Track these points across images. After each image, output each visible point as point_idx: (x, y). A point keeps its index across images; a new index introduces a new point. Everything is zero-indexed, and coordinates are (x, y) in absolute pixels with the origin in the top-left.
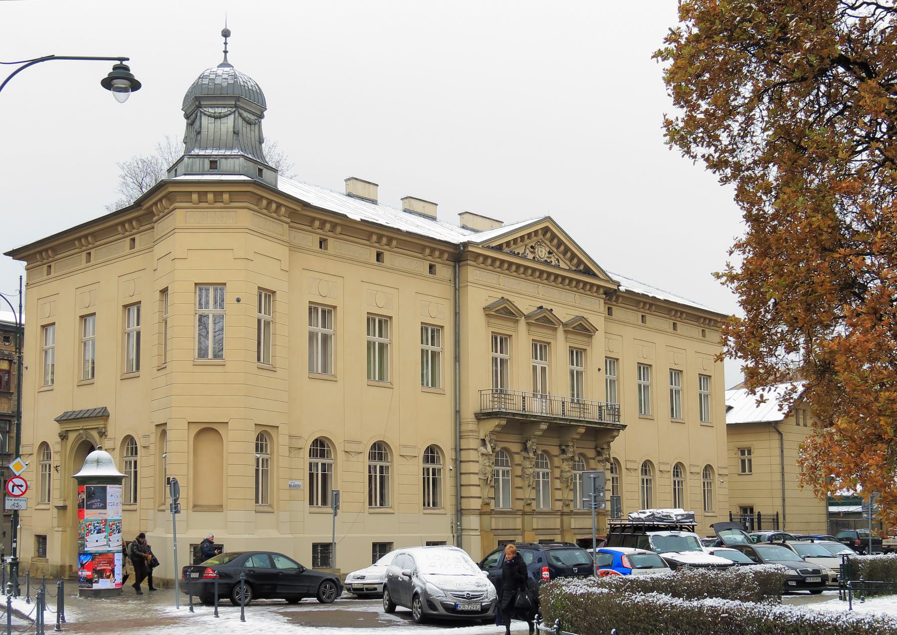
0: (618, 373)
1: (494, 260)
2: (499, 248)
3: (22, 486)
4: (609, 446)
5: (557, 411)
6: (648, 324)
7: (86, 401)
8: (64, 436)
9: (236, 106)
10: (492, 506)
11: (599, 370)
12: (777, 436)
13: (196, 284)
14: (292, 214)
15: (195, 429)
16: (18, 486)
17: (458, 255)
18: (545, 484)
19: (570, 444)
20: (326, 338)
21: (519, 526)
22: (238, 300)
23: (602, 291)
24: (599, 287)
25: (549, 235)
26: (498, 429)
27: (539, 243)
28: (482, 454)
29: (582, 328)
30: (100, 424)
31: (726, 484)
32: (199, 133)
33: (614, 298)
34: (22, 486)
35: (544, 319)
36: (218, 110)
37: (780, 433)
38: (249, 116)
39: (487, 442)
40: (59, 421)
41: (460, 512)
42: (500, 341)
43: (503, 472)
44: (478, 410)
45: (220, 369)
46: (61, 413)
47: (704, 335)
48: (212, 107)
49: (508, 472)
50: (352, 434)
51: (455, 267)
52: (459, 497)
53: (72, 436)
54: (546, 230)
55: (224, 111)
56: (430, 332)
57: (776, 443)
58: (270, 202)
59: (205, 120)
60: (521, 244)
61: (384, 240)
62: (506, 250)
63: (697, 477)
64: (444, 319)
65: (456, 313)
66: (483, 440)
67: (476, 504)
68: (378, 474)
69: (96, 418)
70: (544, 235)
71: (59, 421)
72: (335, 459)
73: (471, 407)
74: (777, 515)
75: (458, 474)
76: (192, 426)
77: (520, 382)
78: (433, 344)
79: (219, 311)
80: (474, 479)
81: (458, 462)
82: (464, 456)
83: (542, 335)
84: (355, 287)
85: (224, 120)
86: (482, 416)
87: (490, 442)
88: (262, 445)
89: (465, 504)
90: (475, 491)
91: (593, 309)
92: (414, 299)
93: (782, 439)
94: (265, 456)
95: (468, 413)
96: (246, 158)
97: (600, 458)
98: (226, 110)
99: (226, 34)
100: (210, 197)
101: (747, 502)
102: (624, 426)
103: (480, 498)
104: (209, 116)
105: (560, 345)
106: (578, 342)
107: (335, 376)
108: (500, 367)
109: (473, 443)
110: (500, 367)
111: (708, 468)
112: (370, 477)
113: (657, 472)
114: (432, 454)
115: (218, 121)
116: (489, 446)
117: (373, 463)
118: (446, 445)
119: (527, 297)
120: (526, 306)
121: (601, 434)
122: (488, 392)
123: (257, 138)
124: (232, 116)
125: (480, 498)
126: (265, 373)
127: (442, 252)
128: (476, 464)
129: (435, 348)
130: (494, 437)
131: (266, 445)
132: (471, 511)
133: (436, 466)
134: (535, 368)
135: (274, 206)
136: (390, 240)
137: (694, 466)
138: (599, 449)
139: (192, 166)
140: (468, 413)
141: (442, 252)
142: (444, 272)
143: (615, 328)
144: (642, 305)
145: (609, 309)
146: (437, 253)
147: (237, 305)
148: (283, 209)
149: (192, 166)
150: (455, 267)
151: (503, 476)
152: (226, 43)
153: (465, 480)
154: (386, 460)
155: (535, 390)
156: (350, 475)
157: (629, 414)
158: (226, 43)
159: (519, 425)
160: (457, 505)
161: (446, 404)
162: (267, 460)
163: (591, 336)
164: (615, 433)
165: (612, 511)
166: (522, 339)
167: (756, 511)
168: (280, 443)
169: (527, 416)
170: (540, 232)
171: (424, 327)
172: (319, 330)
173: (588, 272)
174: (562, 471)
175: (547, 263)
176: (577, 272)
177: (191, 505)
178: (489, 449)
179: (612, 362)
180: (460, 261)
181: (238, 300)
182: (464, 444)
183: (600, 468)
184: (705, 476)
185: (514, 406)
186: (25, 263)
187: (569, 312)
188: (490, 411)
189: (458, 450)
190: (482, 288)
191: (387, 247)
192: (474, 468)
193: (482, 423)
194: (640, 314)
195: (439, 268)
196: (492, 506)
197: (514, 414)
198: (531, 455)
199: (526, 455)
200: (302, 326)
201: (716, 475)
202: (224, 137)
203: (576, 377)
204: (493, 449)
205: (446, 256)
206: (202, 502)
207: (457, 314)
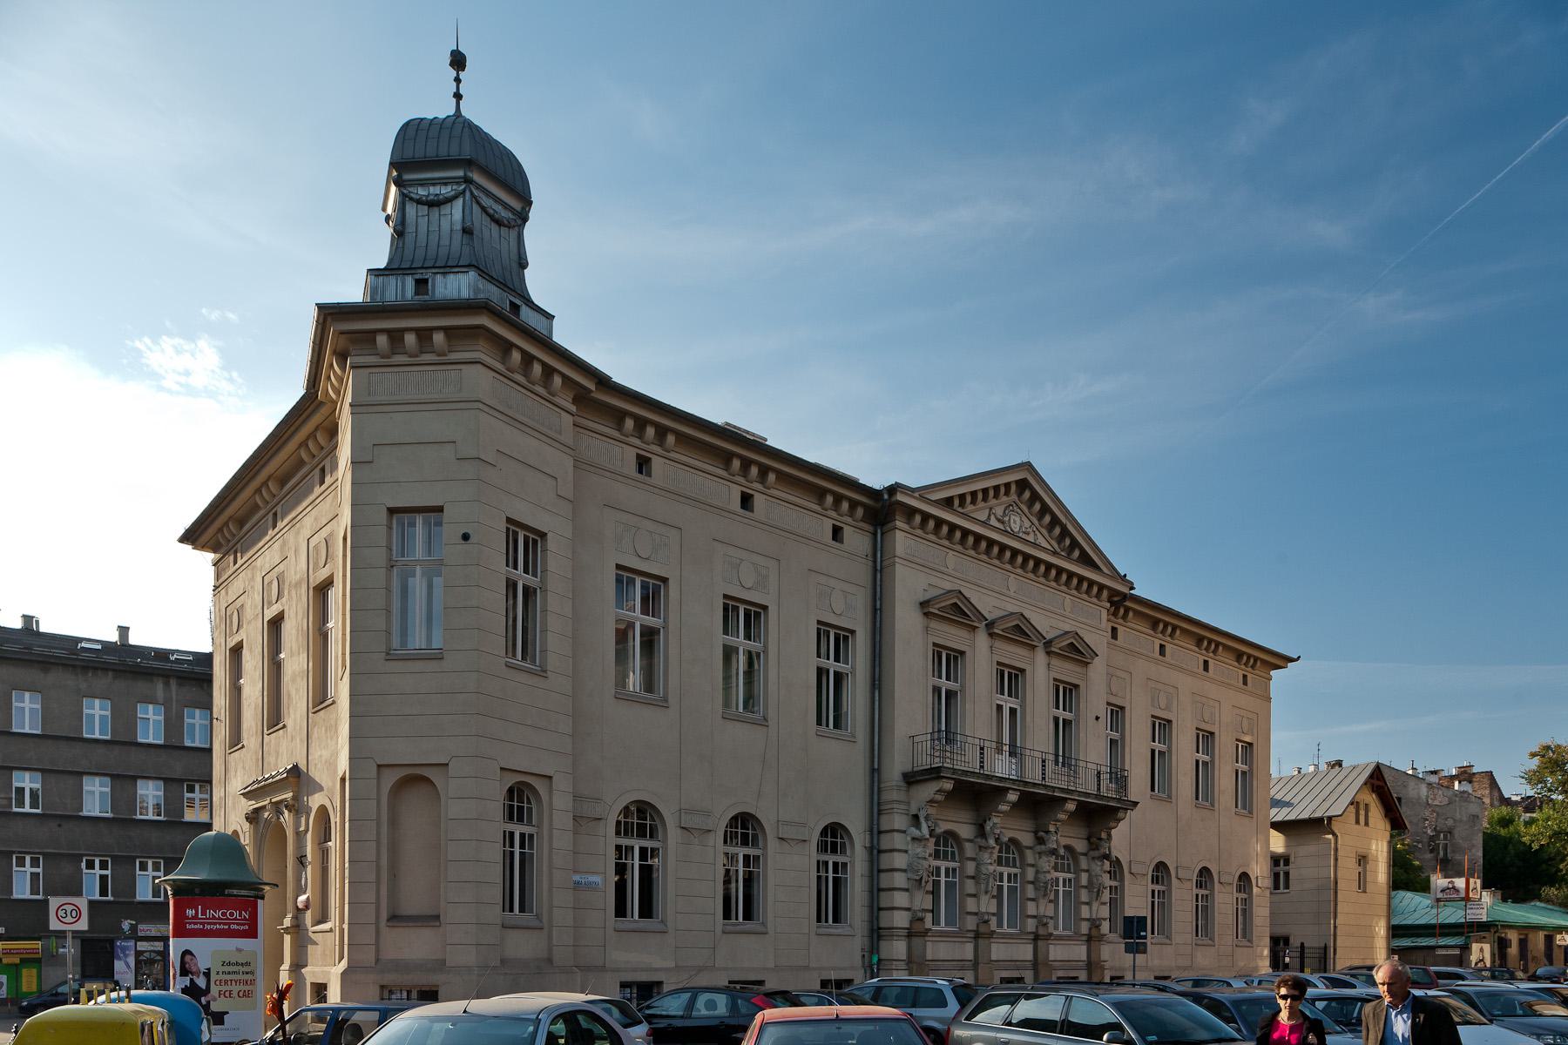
1: (940, 522)
2: (948, 503)
4: (1109, 835)
5: (1033, 774)
14: (582, 398)
15: (391, 778)
17: (881, 509)
18: (1012, 890)
19: (1052, 829)
20: (650, 636)
21: (970, 955)
24: (1102, 587)
25: (1027, 494)
26: (939, 797)
33: (1122, 611)
38: (498, 208)
39: (922, 820)
41: (876, 933)
42: (949, 660)
43: (947, 870)
44: (908, 768)
48: (423, 183)
49: (954, 870)
50: (693, 798)
51: (875, 534)
52: (875, 909)
54: (1023, 485)
55: (446, 191)
56: (834, 639)
58: (396, 336)
60: (982, 504)
65: (875, 610)
66: (916, 817)
67: (901, 920)
68: (831, 875)
70: (1020, 494)
72: (665, 841)
73: (897, 763)
74: (1325, 947)
75: (875, 871)
76: (386, 771)
77: (977, 720)
78: (837, 659)
81: (875, 852)
83: (1014, 655)
84: (709, 551)
85: (446, 209)
86: (912, 779)
87: (927, 818)
88: (520, 809)
90: (900, 899)
91: (1092, 622)
92: (812, 581)
94: (527, 830)
97: (1096, 853)
98: (449, 188)
99: (458, 61)
102: (1136, 804)
103: (908, 909)
104: (419, 202)
108: (948, 701)
109: (899, 821)
110: (948, 701)
112: (819, 878)
114: (833, 837)
116: (924, 826)
117: (824, 857)
119: (996, 592)
121: (1098, 816)
122: (923, 738)
123: (514, 256)
124: (459, 202)
125: (908, 909)
128: (907, 853)
129: (841, 667)
130: (932, 811)
131: (530, 810)
133: (840, 859)
134: (999, 708)
136: (764, 471)
141: (854, 504)
142: (857, 540)
145: (1114, 630)
146: (845, 505)
147: (465, 546)
151: (947, 875)
152: (458, 80)
153: (885, 881)
154: (843, 852)
155: (1000, 743)
156: (692, 872)
157: (1138, 786)
158: (458, 80)
159: (976, 795)
160: (871, 922)
162: (531, 836)
168: (557, 806)
170: (1013, 487)
171: (823, 629)
172: (640, 619)
173: (1086, 560)
174: (1037, 872)
176: (1068, 558)
177: (384, 915)
178: (925, 831)
179: (1117, 713)
180: (883, 525)
183: (1096, 867)
184: (1200, 885)
185: (967, 761)
189: (875, 831)
192: (900, 861)
195: (848, 532)
197: (965, 773)
198: (992, 842)
200: (606, 613)
203: (1064, 729)
204: (932, 833)
205: (860, 512)
206: (408, 909)
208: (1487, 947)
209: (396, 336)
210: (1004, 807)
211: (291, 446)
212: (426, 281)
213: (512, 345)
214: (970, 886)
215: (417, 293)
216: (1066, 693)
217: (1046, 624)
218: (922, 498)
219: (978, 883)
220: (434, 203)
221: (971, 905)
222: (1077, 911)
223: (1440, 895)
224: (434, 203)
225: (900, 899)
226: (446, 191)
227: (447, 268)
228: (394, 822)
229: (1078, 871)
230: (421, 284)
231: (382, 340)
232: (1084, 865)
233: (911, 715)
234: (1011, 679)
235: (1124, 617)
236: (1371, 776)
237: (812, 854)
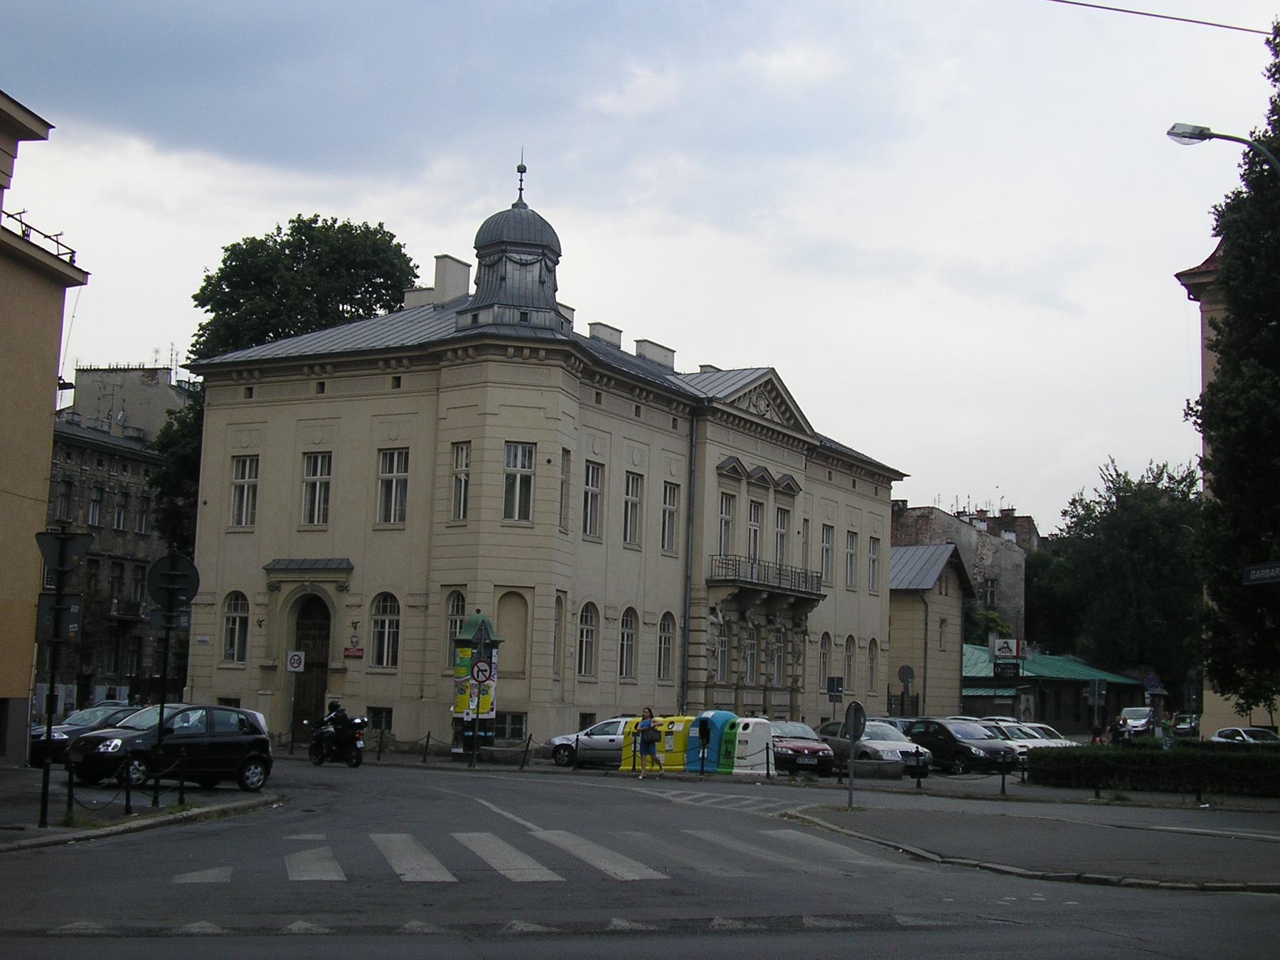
0: (603, 484)
6: (642, 418)
8: (273, 588)
9: (544, 255)
12: (922, 605)
22: (549, 461)
24: (805, 442)
27: (759, 396)
30: (341, 577)
32: (503, 279)
36: (524, 257)
37: (926, 603)
40: (269, 570)
42: (728, 498)
45: (528, 531)
46: (270, 561)
47: (638, 414)
52: (685, 668)
53: (287, 589)
55: (530, 258)
56: (671, 487)
57: (920, 615)
59: (510, 266)
64: (681, 479)
67: (703, 676)
69: (342, 570)
73: (703, 572)
79: (526, 471)
80: (703, 650)
83: (758, 495)
85: (529, 268)
86: (712, 584)
89: (692, 676)
93: (927, 611)
99: (522, 169)
100: (527, 352)
105: (771, 504)
106: (784, 503)
107: (600, 538)
109: (704, 611)
111: (630, 612)
113: (602, 620)
116: (720, 615)
118: (677, 615)
119: (754, 455)
121: (803, 603)
128: (706, 634)
132: (696, 685)
144: (598, 377)
150: (692, 422)
153: (692, 650)
161: (677, 567)
163: (793, 496)
175: (762, 417)
181: (549, 461)
182: (694, 611)
184: (625, 623)
187: (723, 451)
189: (686, 617)
190: (719, 446)
192: (703, 638)
193: (712, 590)
194: (634, 405)
199: (744, 625)
202: (530, 286)
207: (691, 472)
208: (1031, 698)
210: (758, 602)
213: (572, 355)
214: (735, 654)
216: (783, 513)
217: (776, 472)
219: (739, 652)
220: (524, 264)
221: (763, 669)
222: (758, 668)
223: (997, 653)
224: (524, 264)
225: (703, 663)
226: (530, 258)
227: (538, 310)
229: (759, 638)
230: (524, 316)
231: (511, 351)
232: (763, 635)
233: (709, 542)
234: (757, 506)
236: (952, 556)
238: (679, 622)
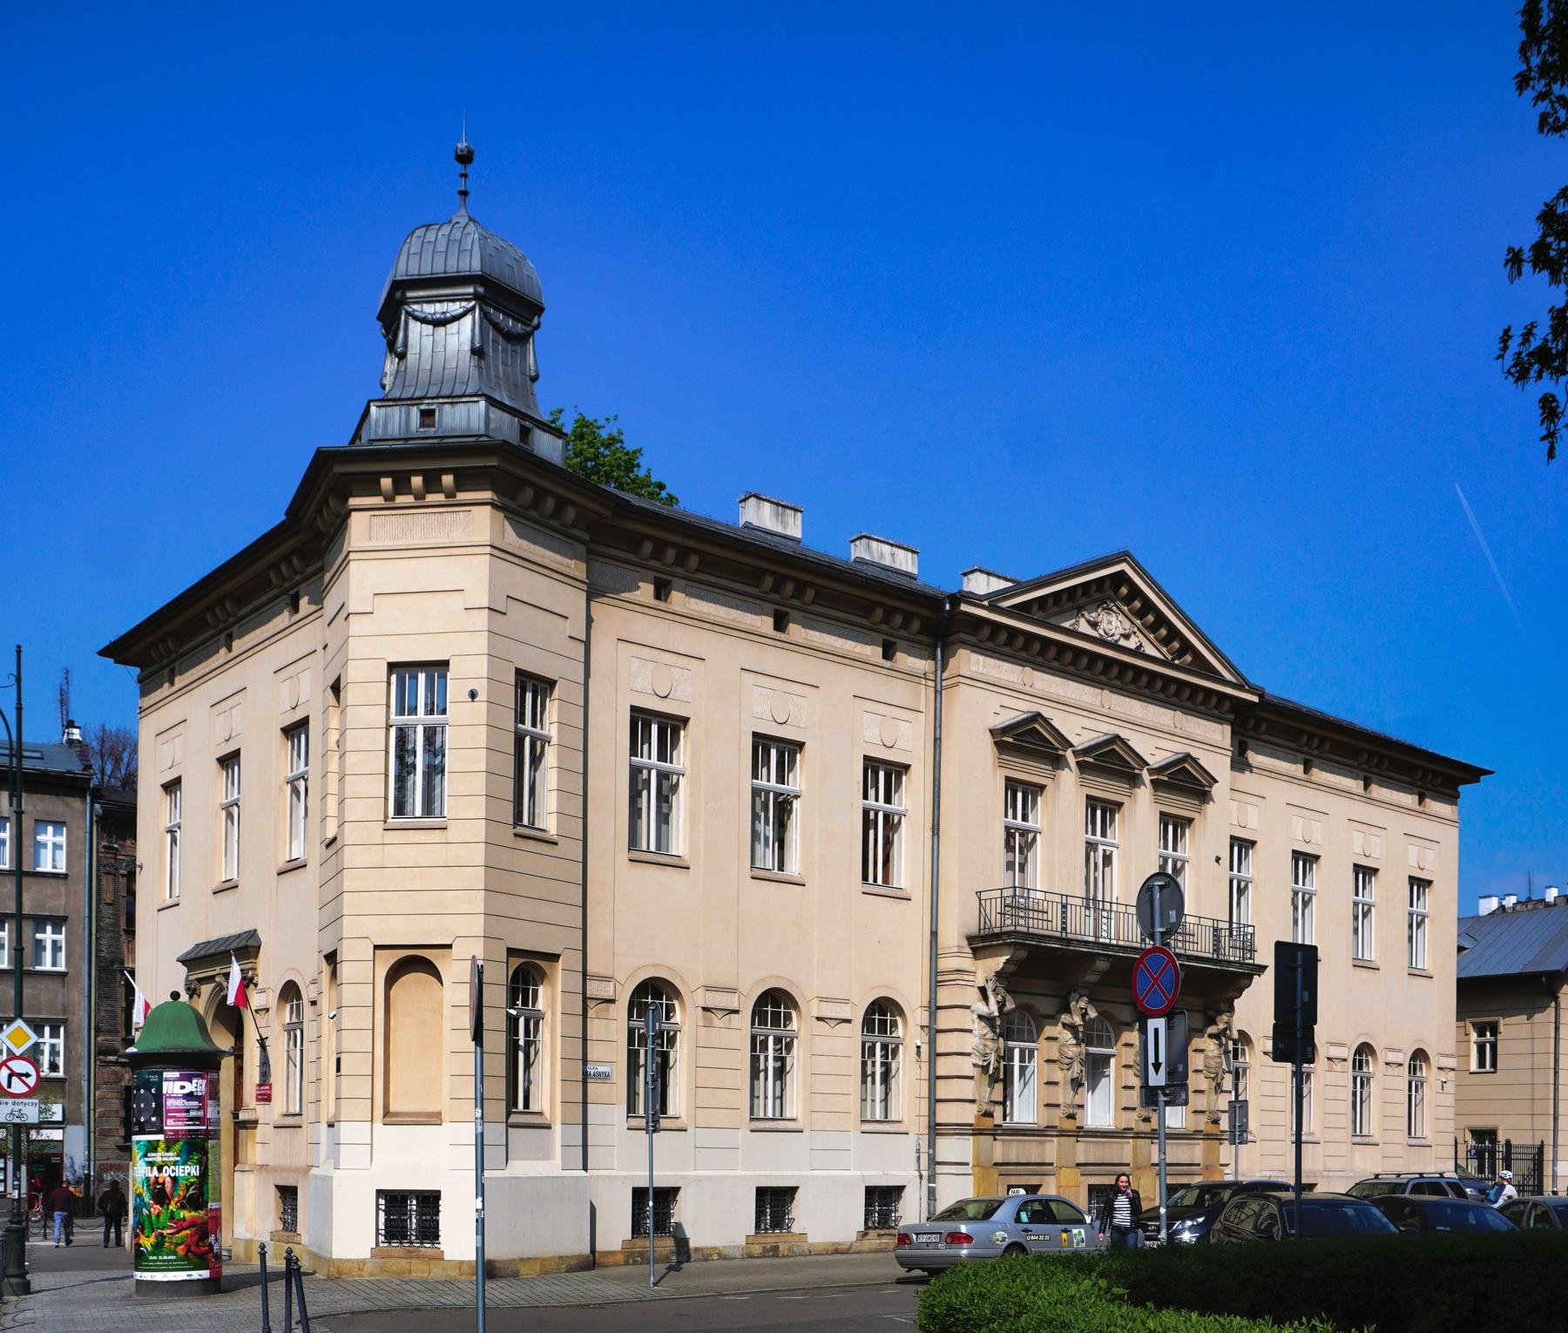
3: (28, 1075)
7: (222, 925)
10: (998, 1119)
11: (1218, 860)
13: (392, 667)
15: (389, 959)
16: (20, 1076)
23: (1227, 705)
28: (980, 1017)
29: (1185, 781)
31: (1450, 1087)
33: (1252, 722)
34: (28, 1075)
35: (1111, 761)
40: (186, 961)
42: (1021, 793)
55: (456, 308)
56: (883, 773)
58: (541, 494)
59: (415, 328)
61: (789, 588)
62: (1039, 615)
63: (1397, 1071)
71: (186, 961)
74: (1541, 1147)
80: (966, 1066)
82: (945, 1020)
85: (452, 327)
86: (981, 944)
91: (1209, 742)
95: (952, 937)
96: (491, 401)
101: (1483, 1123)
103: (973, 1101)
104: (424, 321)
106: (1179, 806)
115: (441, 330)
119: (1082, 713)
120: (1080, 731)
124: (469, 318)
125: (973, 1101)
126: (531, 845)
127: (908, 618)
135: (550, 503)
137: (1393, 1050)
138: (1211, 1013)
139: (385, 424)
140: (952, 937)
141: (908, 618)
143: (1246, 780)
148: (571, 513)
149: (385, 424)
161: (916, 916)
164: (1243, 982)
165: (1232, 1132)
166: (1067, 791)
167: (1501, 1138)
169: (1069, 941)
178: (993, 1009)
186: (136, 671)
188: (997, 930)
191: (796, 602)
196: (998, 1119)
201: (1434, 1069)
205: (916, 625)
207: (937, 741)
209: (541, 494)
211: (258, 566)
212: (433, 411)
215: (422, 425)
218: (993, 608)
227: (453, 398)
228: (506, 1277)
230: (427, 415)
235: (1256, 728)
237: (853, 1035)
238: (916, 1014)
